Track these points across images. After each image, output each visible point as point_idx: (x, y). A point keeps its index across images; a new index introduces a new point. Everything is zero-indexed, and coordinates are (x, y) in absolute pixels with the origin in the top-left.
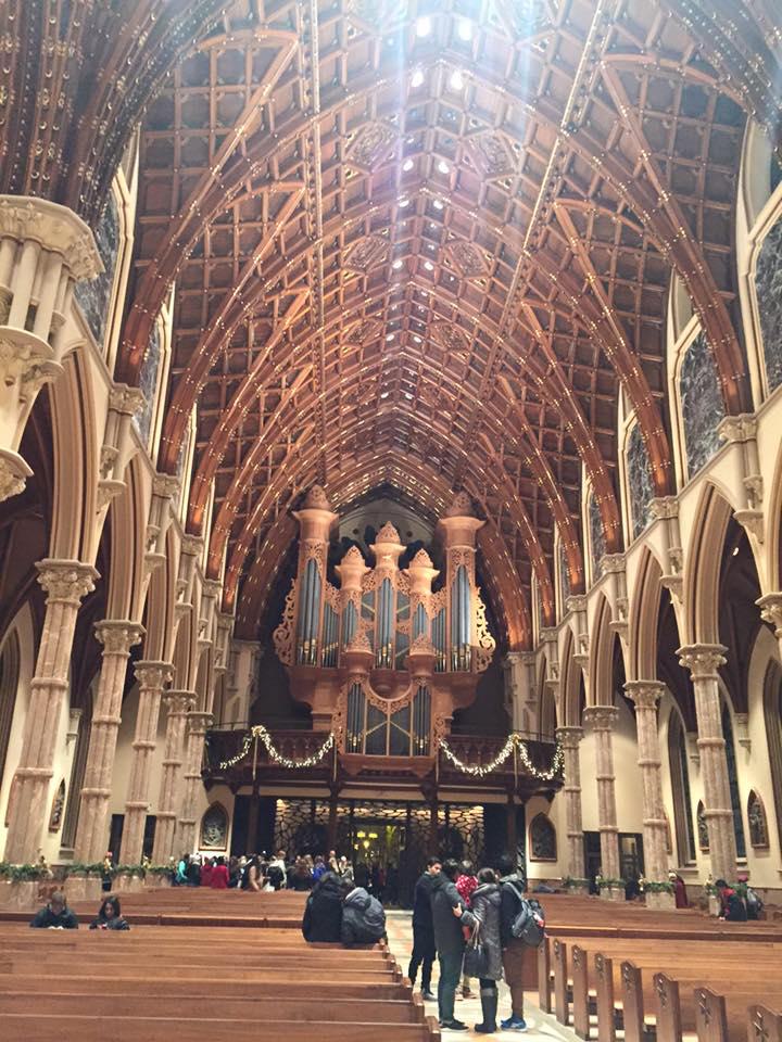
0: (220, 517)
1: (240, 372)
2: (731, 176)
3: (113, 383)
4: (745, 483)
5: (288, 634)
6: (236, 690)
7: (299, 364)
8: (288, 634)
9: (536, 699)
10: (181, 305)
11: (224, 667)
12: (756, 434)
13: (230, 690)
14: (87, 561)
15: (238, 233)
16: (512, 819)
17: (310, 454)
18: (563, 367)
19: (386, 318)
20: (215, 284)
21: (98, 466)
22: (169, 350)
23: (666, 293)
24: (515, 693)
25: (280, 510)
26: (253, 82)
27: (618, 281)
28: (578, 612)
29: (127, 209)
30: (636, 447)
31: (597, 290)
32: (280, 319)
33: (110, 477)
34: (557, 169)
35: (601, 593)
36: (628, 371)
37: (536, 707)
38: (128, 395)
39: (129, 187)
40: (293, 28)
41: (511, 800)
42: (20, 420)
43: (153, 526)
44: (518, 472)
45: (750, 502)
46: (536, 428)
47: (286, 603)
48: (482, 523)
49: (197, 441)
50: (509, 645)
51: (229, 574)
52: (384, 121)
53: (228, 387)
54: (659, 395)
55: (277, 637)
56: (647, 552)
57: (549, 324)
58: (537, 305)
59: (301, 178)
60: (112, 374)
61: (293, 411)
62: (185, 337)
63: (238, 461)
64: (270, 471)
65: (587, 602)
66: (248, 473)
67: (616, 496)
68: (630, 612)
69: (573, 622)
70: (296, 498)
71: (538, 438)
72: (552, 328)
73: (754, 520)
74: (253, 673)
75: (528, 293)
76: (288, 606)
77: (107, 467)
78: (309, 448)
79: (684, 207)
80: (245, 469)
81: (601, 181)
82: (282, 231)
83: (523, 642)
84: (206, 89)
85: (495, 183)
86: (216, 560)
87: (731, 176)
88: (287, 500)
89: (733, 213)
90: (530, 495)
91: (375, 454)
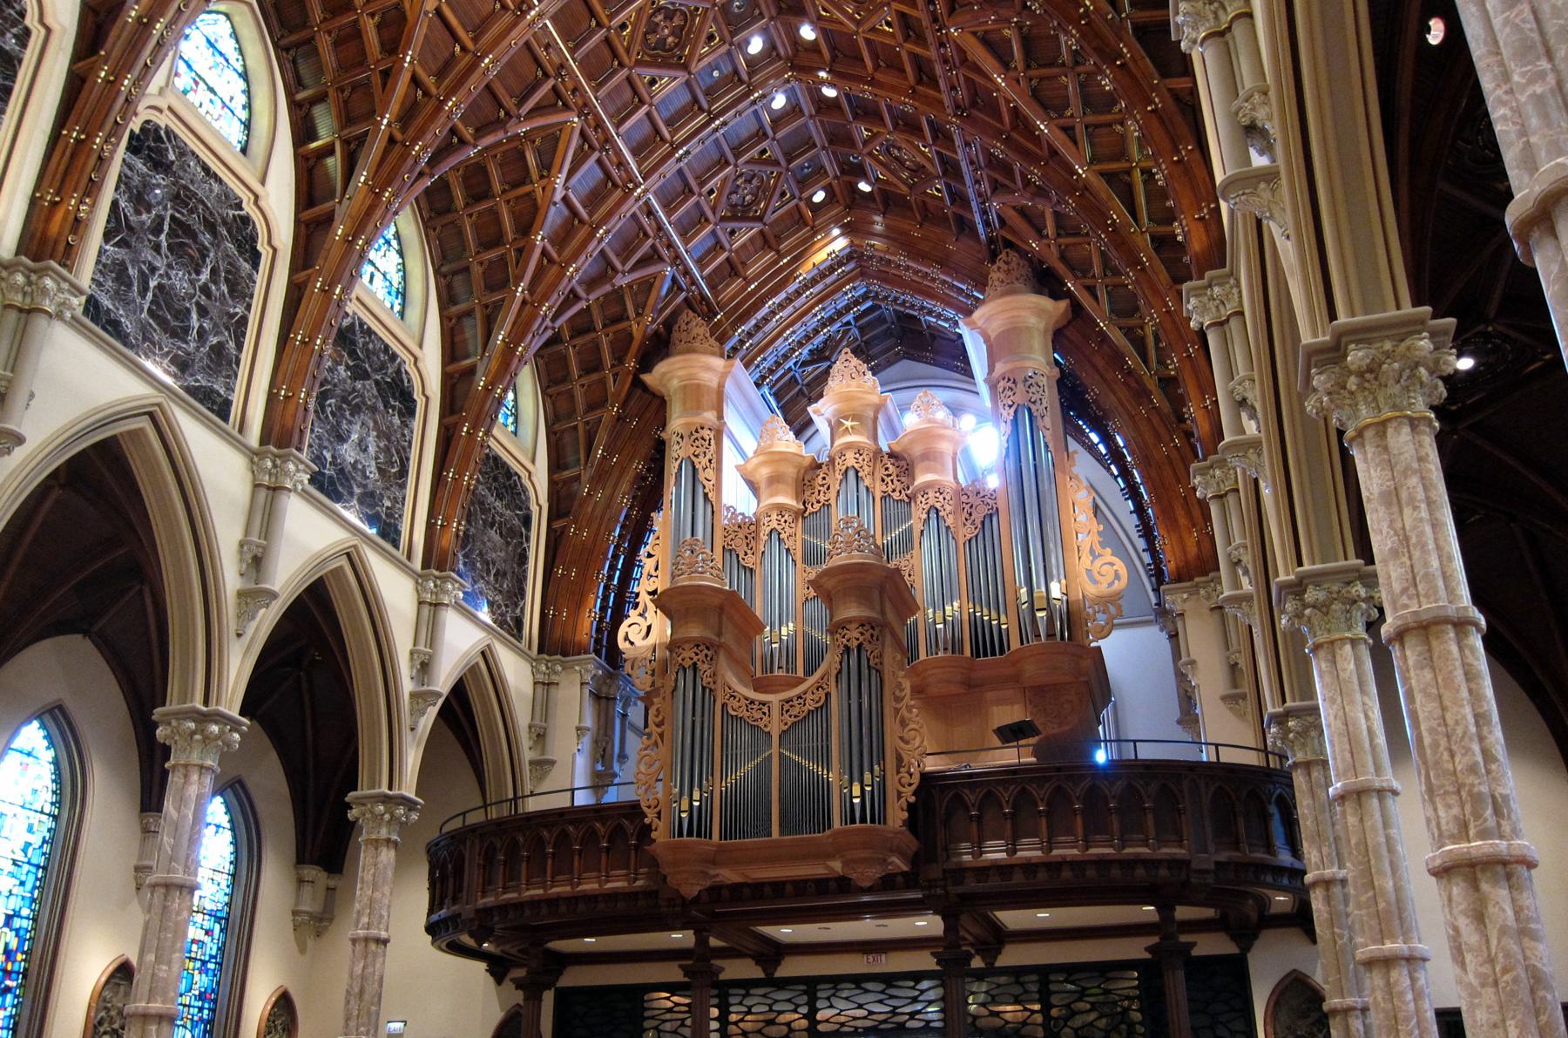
5: (649, 628)
6: (552, 763)
7: (538, 110)
8: (649, 628)
26: (542, 177)
31: (1060, 142)
32: (545, 181)
38: (439, 582)
40: (661, 259)
42: (418, 746)
43: (421, 647)
44: (1097, 270)
55: (626, 638)
61: (468, 58)
70: (642, 343)
71: (1096, 298)
72: (1050, 229)
75: (996, 187)
78: (604, 198)
85: (873, 29)
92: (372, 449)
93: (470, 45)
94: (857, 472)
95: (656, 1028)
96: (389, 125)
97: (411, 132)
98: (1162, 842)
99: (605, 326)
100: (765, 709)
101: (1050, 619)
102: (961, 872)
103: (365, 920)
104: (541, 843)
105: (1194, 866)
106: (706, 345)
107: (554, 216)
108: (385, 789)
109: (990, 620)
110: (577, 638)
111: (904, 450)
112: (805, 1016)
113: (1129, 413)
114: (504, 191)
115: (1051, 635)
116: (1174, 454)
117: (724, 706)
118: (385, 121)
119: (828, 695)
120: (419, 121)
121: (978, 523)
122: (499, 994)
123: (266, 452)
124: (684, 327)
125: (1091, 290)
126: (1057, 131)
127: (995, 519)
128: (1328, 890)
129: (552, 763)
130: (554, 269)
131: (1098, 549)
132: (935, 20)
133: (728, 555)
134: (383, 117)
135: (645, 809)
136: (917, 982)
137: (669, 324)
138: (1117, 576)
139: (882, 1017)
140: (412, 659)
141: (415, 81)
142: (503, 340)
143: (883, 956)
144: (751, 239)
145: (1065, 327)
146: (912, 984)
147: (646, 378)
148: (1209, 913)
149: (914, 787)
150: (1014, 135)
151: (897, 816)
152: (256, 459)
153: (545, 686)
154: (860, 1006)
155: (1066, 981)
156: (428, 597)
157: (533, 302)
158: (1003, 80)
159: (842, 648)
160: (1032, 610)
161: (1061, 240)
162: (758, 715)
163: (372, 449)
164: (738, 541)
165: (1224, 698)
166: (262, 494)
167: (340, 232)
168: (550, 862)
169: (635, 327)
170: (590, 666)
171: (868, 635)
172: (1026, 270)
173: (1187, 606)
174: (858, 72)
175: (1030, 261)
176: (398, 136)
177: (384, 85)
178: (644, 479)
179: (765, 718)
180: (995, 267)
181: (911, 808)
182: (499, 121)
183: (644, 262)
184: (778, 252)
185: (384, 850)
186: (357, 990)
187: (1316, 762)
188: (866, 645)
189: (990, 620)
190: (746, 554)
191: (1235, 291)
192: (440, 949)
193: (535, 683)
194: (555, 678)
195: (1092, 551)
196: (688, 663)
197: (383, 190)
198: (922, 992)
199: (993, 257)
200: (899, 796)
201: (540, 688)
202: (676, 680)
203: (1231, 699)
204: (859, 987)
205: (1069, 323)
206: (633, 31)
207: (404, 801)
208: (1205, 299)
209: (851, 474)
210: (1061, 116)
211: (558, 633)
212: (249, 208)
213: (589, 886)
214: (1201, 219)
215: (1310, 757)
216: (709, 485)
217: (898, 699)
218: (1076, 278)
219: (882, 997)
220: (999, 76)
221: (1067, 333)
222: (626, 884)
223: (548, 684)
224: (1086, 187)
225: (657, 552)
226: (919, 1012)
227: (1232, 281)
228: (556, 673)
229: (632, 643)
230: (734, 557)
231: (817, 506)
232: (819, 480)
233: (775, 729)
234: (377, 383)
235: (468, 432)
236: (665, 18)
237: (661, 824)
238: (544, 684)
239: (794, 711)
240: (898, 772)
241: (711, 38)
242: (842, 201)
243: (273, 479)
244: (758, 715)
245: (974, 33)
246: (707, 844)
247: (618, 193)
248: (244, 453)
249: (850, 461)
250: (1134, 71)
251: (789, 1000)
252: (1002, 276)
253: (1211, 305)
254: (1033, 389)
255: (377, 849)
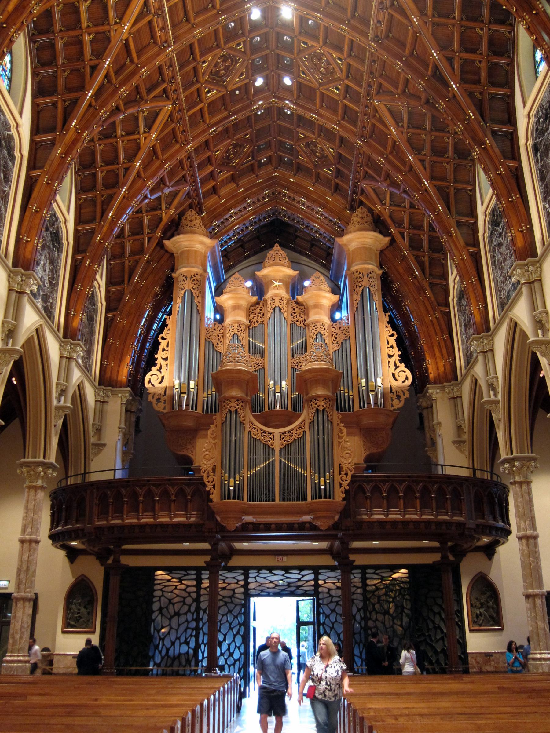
0: (34, 195)
1: (113, 187)
2: (471, 166)
3: (63, 340)
4: (535, 317)
5: (163, 377)
6: (104, 445)
8: (163, 377)
9: (465, 437)
10: (80, 205)
11: (69, 404)
12: (540, 276)
13: (94, 445)
14: (49, 459)
15: (121, 145)
16: (448, 578)
17: (172, 156)
18: (400, 233)
19: (248, 52)
20: (107, 186)
21: (55, 395)
22: (104, 303)
23: (511, 64)
24: (439, 432)
25: (149, 239)
26: (145, 132)
27: (411, 231)
28: (484, 352)
29: (68, 224)
30: (461, 295)
31: (418, 166)
32: (146, 135)
33: (62, 403)
34: (371, 73)
35: (512, 319)
36: (480, 143)
37: (467, 447)
39: (68, 212)
41: (444, 557)
43: (61, 381)
45: (540, 332)
46: (402, 230)
47: (159, 343)
48: (387, 239)
49: (106, 312)
50: (428, 377)
51: (73, 295)
52: (231, 48)
53: (103, 202)
54: (473, 250)
55: (150, 382)
56: (474, 382)
57: (385, 199)
58: (373, 184)
59: (185, 181)
60: (61, 335)
61: (133, 66)
62: (114, 292)
63: (98, 215)
64: (122, 172)
65: (540, 267)
66: (75, 142)
67: (522, 196)
68: (500, 389)
69: (479, 370)
70: (167, 224)
71: (404, 238)
72: (388, 201)
73: (543, 347)
74: (123, 426)
76: (161, 347)
77: (60, 395)
79: (471, 95)
80: (70, 135)
81: (407, 81)
82: (129, 34)
83: (445, 373)
84: (114, 140)
85: (328, 89)
86: (29, 247)
87: (471, 166)
88: (157, 227)
89: (512, 96)
90: (443, 179)
91: (258, 177)
92: (47, 270)
93: (136, 60)
94: (280, 309)
95: (161, 590)
96: (91, 97)
97: (99, 101)
98: (454, 514)
99: (147, 211)
100: (272, 436)
101: (376, 396)
102: (362, 522)
103: (29, 530)
104: (135, 495)
105: (467, 526)
106: (200, 230)
107: (115, 47)
108: (41, 459)
109: (344, 393)
110: (119, 379)
111: (304, 301)
112: (242, 586)
113: (414, 297)
114: (122, 136)
115: (376, 404)
116: (435, 321)
117: (250, 432)
118: (90, 94)
119: (304, 432)
120: (104, 96)
121: (340, 343)
122: (71, 568)
123: (19, 272)
124: (189, 218)
125: (402, 234)
126: (418, 162)
127: (348, 341)
128: (528, 541)
129: (104, 445)
130: (141, 181)
131: (398, 364)
132: (368, 95)
133: (207, 343)
134: (89, 92)
135: (207, 483)
136: (301, 571)
137: (181, 215)
138: (407, 378)
139: (281, 588)
140: (57, 387)
141: (107, 76)
142: (112, 216)
143: (286, 558)
144: (227, 178)
145: (385, 249)
146: (298, 572)
147: (167, 243)
148: (436, 544)
149: (348, 482)
150: (390, 156)
151: (339, 495)
152: (12, 275)
153: (101, 403)
154: (271, 582)
155: (374, 573)
156: (66, 354)
157: (128, 197)
158: (396, 131)
159: (315, 409)
160: (368, 391)
161: (392, 208)
162: (268, 439)
163: (47, 270)
164: (213, 337)
165: (454, 442)
166: (14, 295)
167: (59, 151)
168: (141, 505)
169: (164, 214)
170: (126, 394)
171: (328, 404)
172: (370, 219)
173: (437, 396)
174: (313, 107)
175: (373, 215)
176: (94, 103)
177: (91, 75)
178: (157, 295)
179: (272, 441)
180: (355, 214)
181: (346, 492)
182: (136, 100)
183: (178, 183)
184: (238, 185)
185: (39, 491)
186: (25, 568)
187: (524, 482)
188: (327, 409)
189: (344, 393)
190: (218, 344)
191: (539, 269)
192: (56, 547)
193: (96, 401)
194: (106, 399)
195: (395, 364)
196: (233, 409)
197: (83, 132)
198: (303, 576)
199: (353, 209)
200: (341, 485)
201: (98, 404)
202: (226, 418)
203: (458, 443)
204: (271, 572)
205: (387, 247)
206: (208, 65)
207: (50, 466)
208: (524, 270)
209: (277, 310)
210: (419, 154)
211: (108, 375)
212: (14, 132)
213: (164, 519)
214: (522, 231)
215: (522, 479)
216: (199, 305)
217: (340, 437)
218: (396, 227)
219: (283, 578)
220: (394, 128)
221: (386, 252)
222: (185, 519)
223: (103, 402)
224: (426, 190)
225: (168, 337)
226: (301, 586)
227: (538, 265)
228: (108, 396)
229: (153, 385)
230: (211, 346)
231: (257, 324)
232: (258, 310)
233: (277, 446)
234: (51, 233)
235: (89, 265)
236: (223, 61)
237: (215, 492)
238: (100, 402)
239: (287, 439)
240: (340, 474)
241: (242, 74)
242: (274, 164)
243: (19, 287)
244: (268, 439)
245: (385, 105)
246: (241, 503)
247: (178, 146)
248: (6, 270)
249: (277, 304)
250: (492, 153)
251: (234, 578)
252: (359, 220)
253: (526, 273)
254: (371, 280)
255: (36, 491)
